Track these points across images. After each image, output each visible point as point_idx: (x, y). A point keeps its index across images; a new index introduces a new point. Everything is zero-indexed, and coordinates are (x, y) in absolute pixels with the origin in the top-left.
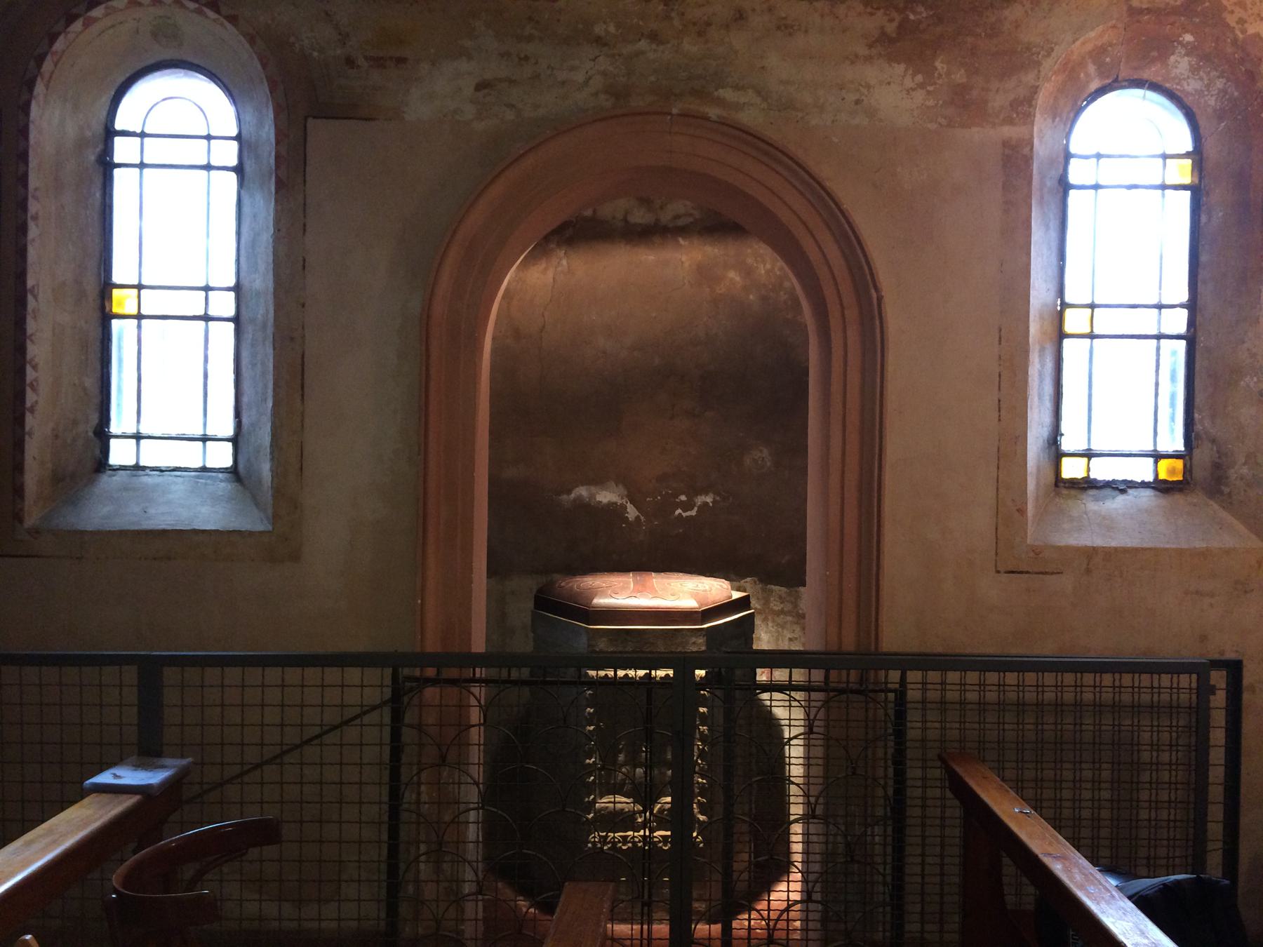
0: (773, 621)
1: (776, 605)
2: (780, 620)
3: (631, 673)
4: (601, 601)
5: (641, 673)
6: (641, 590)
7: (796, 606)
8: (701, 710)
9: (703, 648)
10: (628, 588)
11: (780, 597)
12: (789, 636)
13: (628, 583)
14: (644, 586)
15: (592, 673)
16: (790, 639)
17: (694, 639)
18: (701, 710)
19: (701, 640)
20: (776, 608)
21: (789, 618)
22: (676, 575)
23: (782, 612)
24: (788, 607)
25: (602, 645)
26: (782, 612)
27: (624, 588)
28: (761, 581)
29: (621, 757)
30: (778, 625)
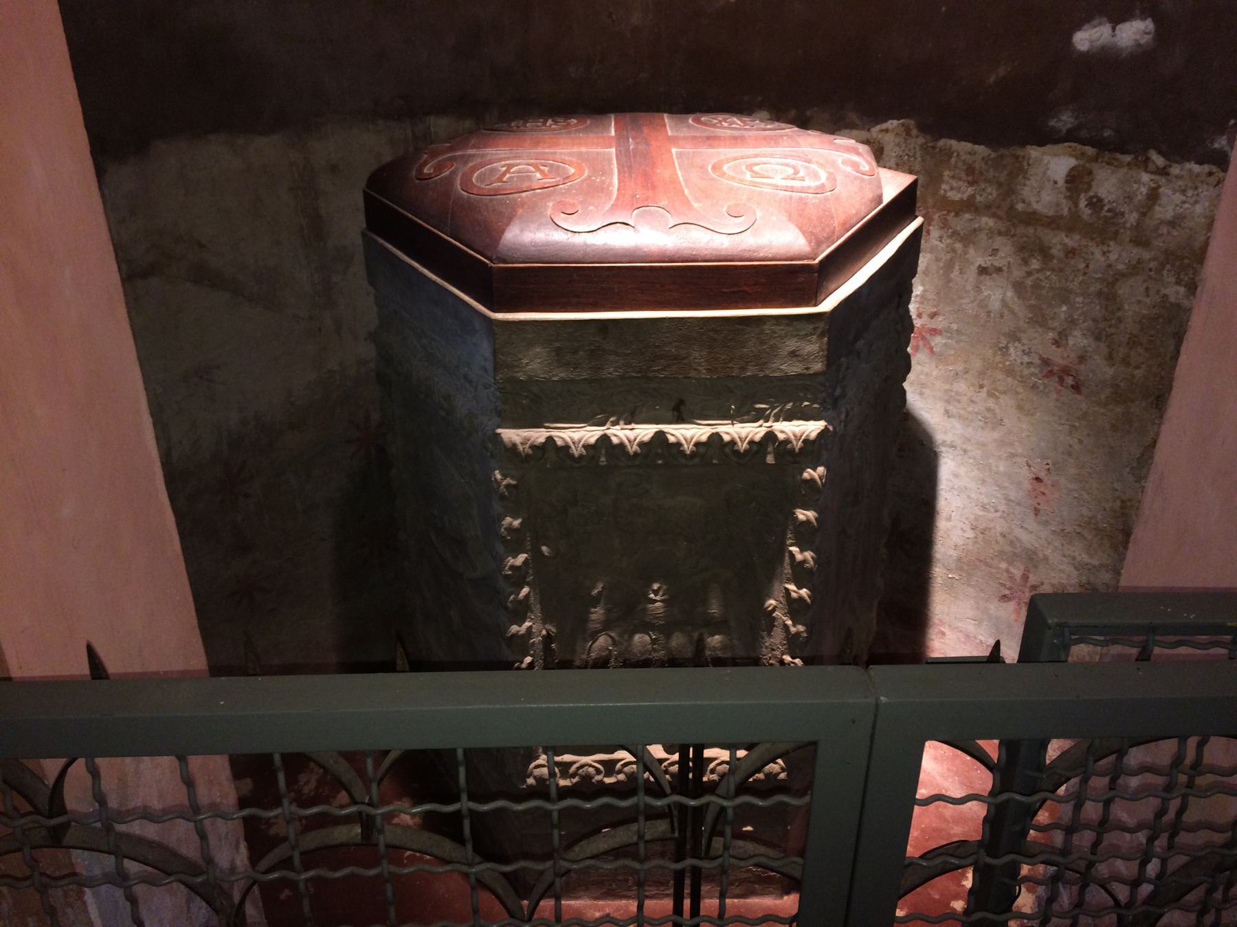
0: (945, 225)
1: (955, 189)
2: (962, 223)
3: (620, 433)
4: (537, 234)
5: (645, 432)
6: (644, 187)
7: (1008, 190)
8: (802, 515)
9: (818, 367)
10: (603, 189)
11: (970, 170)
12: (980, 261)
13: (599, 167)
14: (649, 182)
15: (510, 435)
16: (983, 271)
17: (792, 344)
18: (802, 515)
19: (813, 347)
20: (954, 196)
21: (987, 222)
22: (729, 125)
23: (969, 205)
24: (991, 193)
25: (535, 363)
26: (969, 205)
27: (594, 191)
28: (923, 128)
29: (597, 613)
30: (955, 234)
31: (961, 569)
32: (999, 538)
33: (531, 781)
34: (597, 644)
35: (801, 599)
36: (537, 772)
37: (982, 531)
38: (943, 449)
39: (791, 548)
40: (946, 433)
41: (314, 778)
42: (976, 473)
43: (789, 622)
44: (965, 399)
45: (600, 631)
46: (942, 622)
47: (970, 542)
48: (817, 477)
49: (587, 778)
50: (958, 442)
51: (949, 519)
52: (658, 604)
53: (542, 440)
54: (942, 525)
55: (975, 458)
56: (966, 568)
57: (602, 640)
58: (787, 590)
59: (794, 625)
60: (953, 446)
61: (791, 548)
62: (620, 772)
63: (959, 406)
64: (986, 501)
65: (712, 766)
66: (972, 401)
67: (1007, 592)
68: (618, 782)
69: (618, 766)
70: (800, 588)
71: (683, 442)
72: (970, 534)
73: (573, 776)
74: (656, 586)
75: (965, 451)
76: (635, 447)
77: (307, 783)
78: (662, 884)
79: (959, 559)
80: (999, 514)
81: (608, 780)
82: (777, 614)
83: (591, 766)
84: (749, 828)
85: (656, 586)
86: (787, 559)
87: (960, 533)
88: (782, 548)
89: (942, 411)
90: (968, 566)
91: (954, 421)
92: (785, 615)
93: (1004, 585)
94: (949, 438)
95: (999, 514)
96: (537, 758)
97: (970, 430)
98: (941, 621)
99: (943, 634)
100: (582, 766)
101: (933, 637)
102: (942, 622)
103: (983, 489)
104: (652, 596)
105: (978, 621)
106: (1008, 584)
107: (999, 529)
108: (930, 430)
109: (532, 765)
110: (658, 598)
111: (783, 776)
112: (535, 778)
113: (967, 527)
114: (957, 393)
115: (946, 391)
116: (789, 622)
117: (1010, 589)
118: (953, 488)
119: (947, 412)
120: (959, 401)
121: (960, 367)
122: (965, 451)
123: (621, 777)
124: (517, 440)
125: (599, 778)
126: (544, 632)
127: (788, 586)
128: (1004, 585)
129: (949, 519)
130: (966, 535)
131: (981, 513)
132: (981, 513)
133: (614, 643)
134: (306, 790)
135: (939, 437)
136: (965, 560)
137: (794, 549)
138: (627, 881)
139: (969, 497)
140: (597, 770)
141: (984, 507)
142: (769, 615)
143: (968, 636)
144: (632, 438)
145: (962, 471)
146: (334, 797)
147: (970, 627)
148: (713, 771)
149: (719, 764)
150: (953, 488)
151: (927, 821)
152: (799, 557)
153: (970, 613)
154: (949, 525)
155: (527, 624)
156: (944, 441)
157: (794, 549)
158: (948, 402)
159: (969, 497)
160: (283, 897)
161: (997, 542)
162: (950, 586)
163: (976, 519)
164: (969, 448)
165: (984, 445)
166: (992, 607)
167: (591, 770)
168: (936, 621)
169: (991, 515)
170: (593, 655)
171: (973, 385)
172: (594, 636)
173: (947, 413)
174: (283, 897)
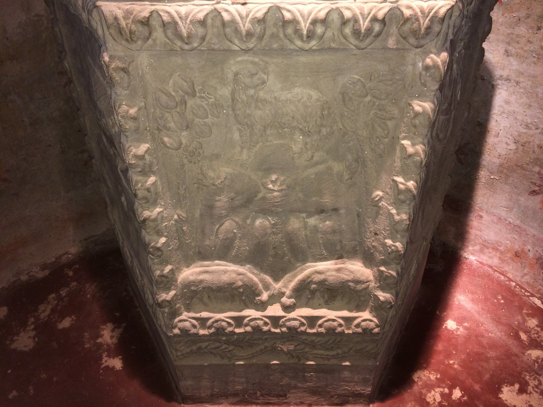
31: (502, 172)
32: (536, 149)
33: (176, 331)
34: (223, 227)
35: (408, 190)
36: (180, 325)
37: (521, 144)
38: (499, 82)
39: (403, 142)
40: (503, 69)
41: (50, 307)
42: (524, 100)
43: (394, 211)
44: (523, 40)
45: (227, 216)
46: (481, 209)
47: (512, 152)
48: (440, 63)
49: (220, 331)
50: (513, 76)
51: (497, 136)
52: (276, 194)
53: (146, 14)
54: (490, 140)
55: (525, 88)
56: (505, 171)
57: (228, 224)
58: (394, 181)
59: (398, 214)
60: (508, 79)
61: (403, 142)
62: (247, 325)
63: (517, 46)
64: (529, 121)
65: (320, 322)
66: (529, 42)
67: (537, 188)
68: (246, 332)
69: (246, 321)
70: (407, 180)
71: (300, 19)
72: (513, 146)
73: (210, 327)
74: (274, 177)
75: (518, 83)
76: (248, 25)
77: (44, 311)
78: (281, 396)
79: (501, 165)
80: (539, 131)
81: (237, 331)
82: (383, 203)
83: (223, 321)
84: (347, 363)
85: (274, 177)
86: (398, 148)
87: (505, 146)
88: (395, 140)
89: (502, 51)
90: (508, 169)
91: (512, 59)
92: (391, 204)
93: (535, 184)
94: (505, 73)
95: (539, 131)
96: (180, 314)
97: (524, 65)
98: (480, 208)
99: (481, 217)
100: (217, 321)
101: (473, 219)
102: (481, 209)
103: (528, 112)
104: (270, 186)
105: (510, 209)
106: (538, 182)
107: (537, 142)
108: (490, 67)
109: (176, 320)
110: (276, 188)
111: (376, 330)
112: (179, 329)
113: (511, 142)
114: (517, 36)
115: (508, 34)
116: (394, 211)
117: (539, 186)
118: (503, 112)
119: (506, 51)
120: (518, 43)
121: (522, 13)
122: (518, 83)
123: (248, 329)
124: (120, 14)
125: (230, 329)
126: (176, 217)
127: (396, 178)
128: (535, 184)
129: (497, 136)
130: (509, 147)
131: (525, 131)
132: (525, 131)
133: (240, 227)
134: (42, 316)
135: (498, 73)
136: (506, 165)
137: (406, 142)
138: (256, 394)
139: (516, 118)
140: (229, 323)
141: (527, 126)
142: (376, 204)
143: (500, 219)
144: (244, 13)
145: (513, 99)
146: (61, 322)
147: (503, 213)
148: (320, 326)
149: (326, 321)
150: (503, 112)
151: (471, 347)
152: (410, 150)
153: (504, 203)
154: (496, 140)
155: (158, 210)
156: (501, 76)
157: (406, 142)
158: (509, 44)
159: (516, 118)
160: (10, 396)
161: (534, 152)
162: (491, 184)
163: (519, 135)
164: (521, 80)
165: (535, 77)
166: (522, 199)
167: (224, 324)
168: (477, 208)
169: (531, 132)
170: (221, 236)
171: (531, 28)
172: (221, 219)
173: (507, 53)
174: (10, 396)
